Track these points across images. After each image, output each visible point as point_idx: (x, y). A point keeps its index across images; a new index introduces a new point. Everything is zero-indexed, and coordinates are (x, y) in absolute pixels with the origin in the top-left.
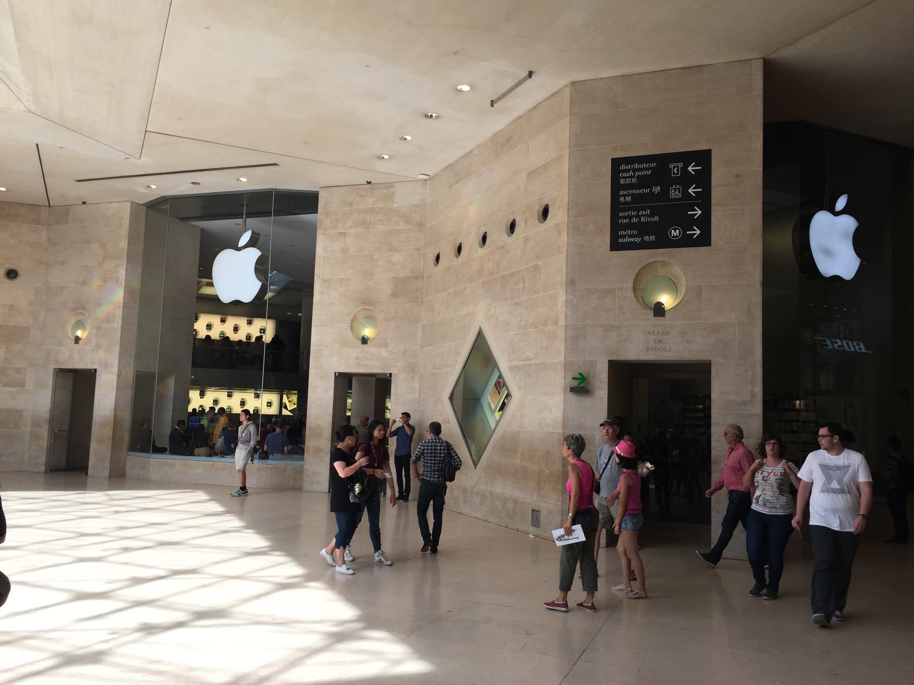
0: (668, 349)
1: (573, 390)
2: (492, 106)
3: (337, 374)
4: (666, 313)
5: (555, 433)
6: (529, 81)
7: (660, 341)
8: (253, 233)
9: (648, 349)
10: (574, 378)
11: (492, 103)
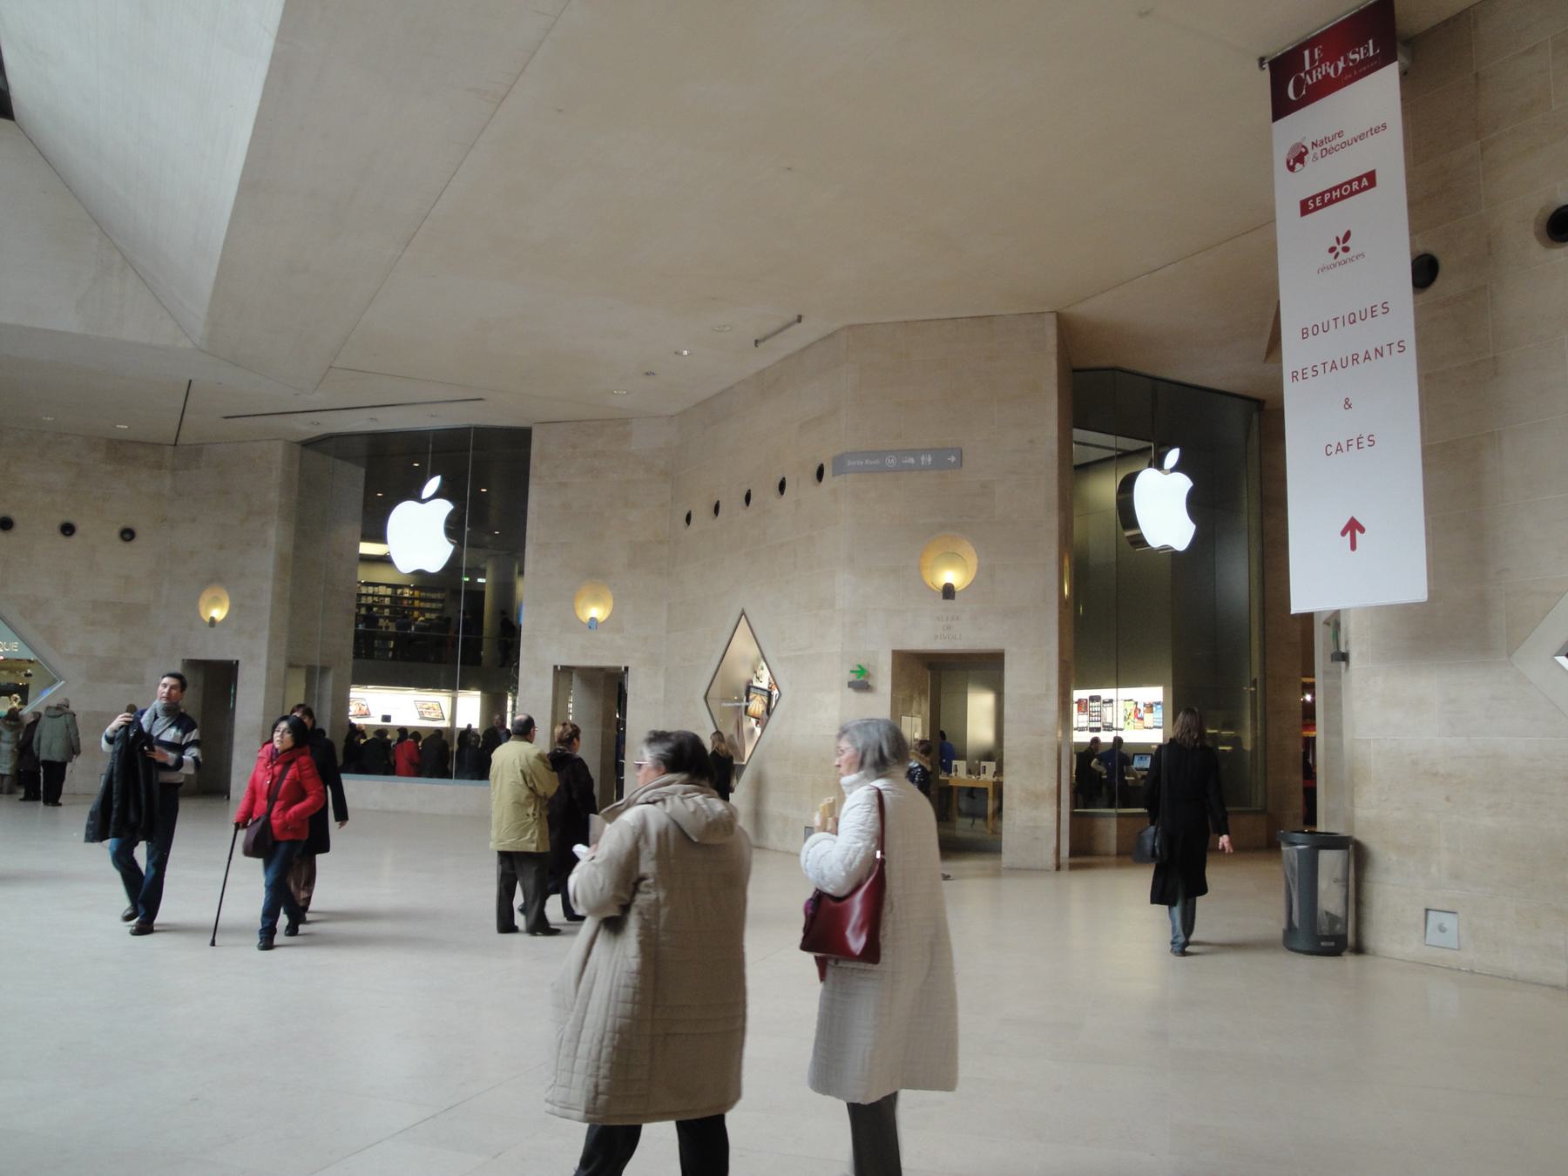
0: (958, 637)
1: (851, 685)
2: (756, 346)
3: (559, 668)
4: (956, 595)
5: (830, 736)
6: (798, 326)
7: (949, 628)
8: (1296, 929)
9: (936, 637)
10: (852, 672)
11: (757, 342)
